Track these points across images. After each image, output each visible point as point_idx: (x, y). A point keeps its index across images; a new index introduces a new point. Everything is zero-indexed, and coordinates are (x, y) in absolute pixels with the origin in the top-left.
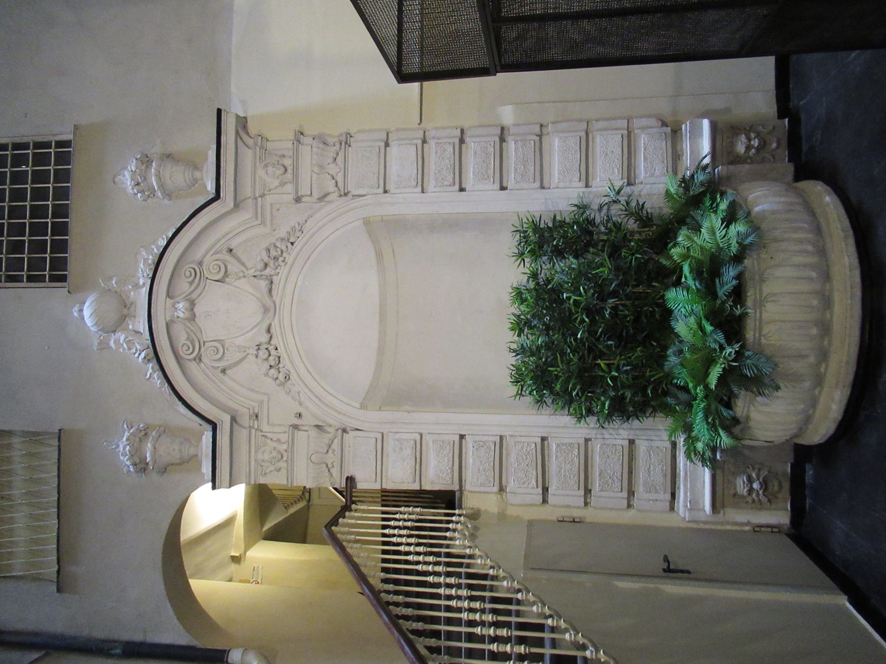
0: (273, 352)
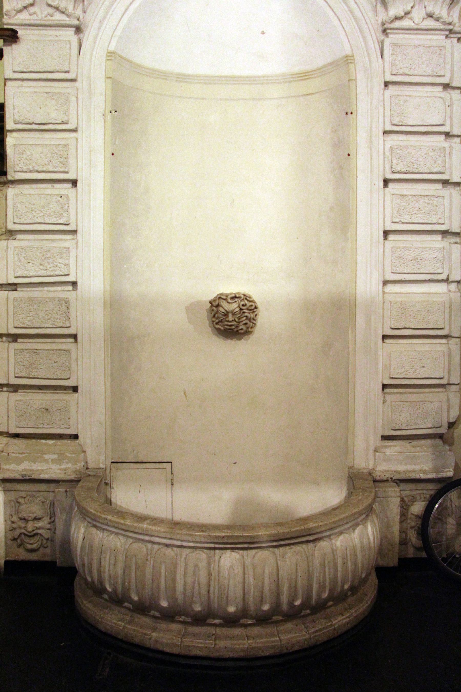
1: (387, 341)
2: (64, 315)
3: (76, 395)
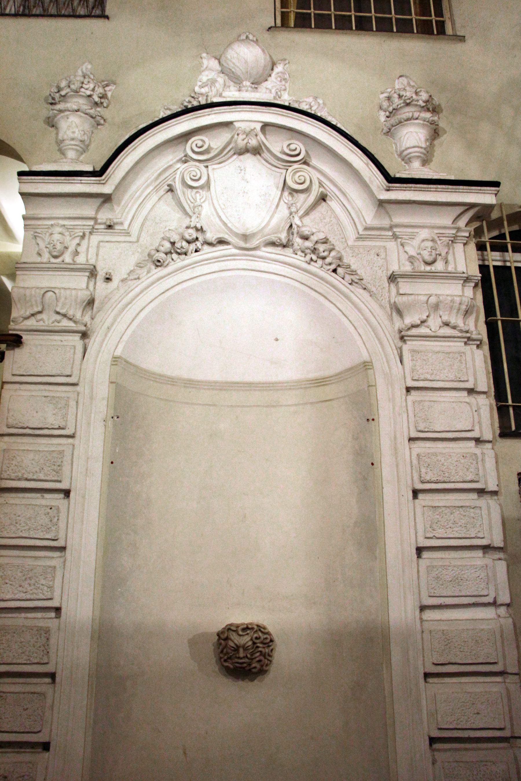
0: (193, 247)
1: (430, 680)
2: (42, 648)
3: (46, 755)
